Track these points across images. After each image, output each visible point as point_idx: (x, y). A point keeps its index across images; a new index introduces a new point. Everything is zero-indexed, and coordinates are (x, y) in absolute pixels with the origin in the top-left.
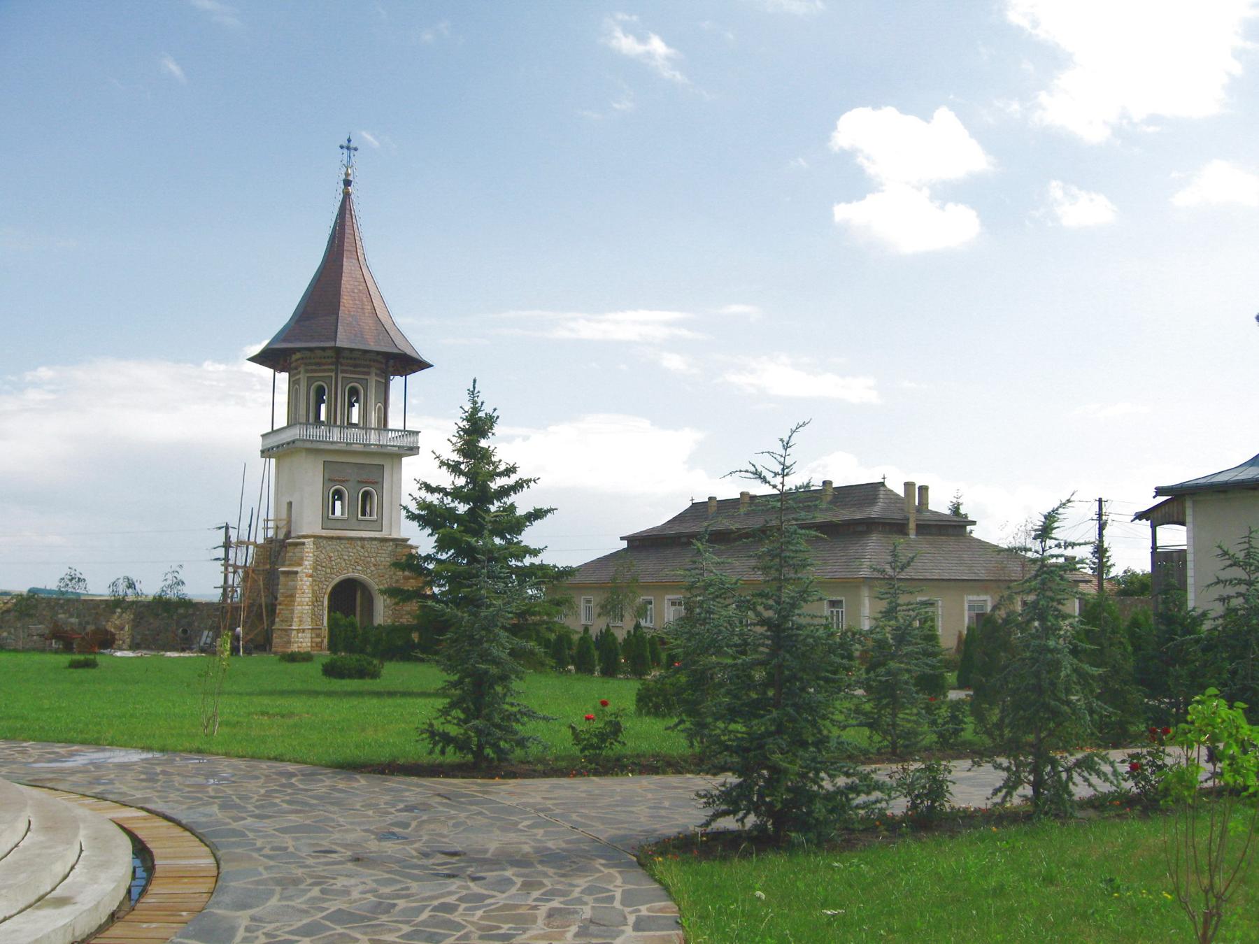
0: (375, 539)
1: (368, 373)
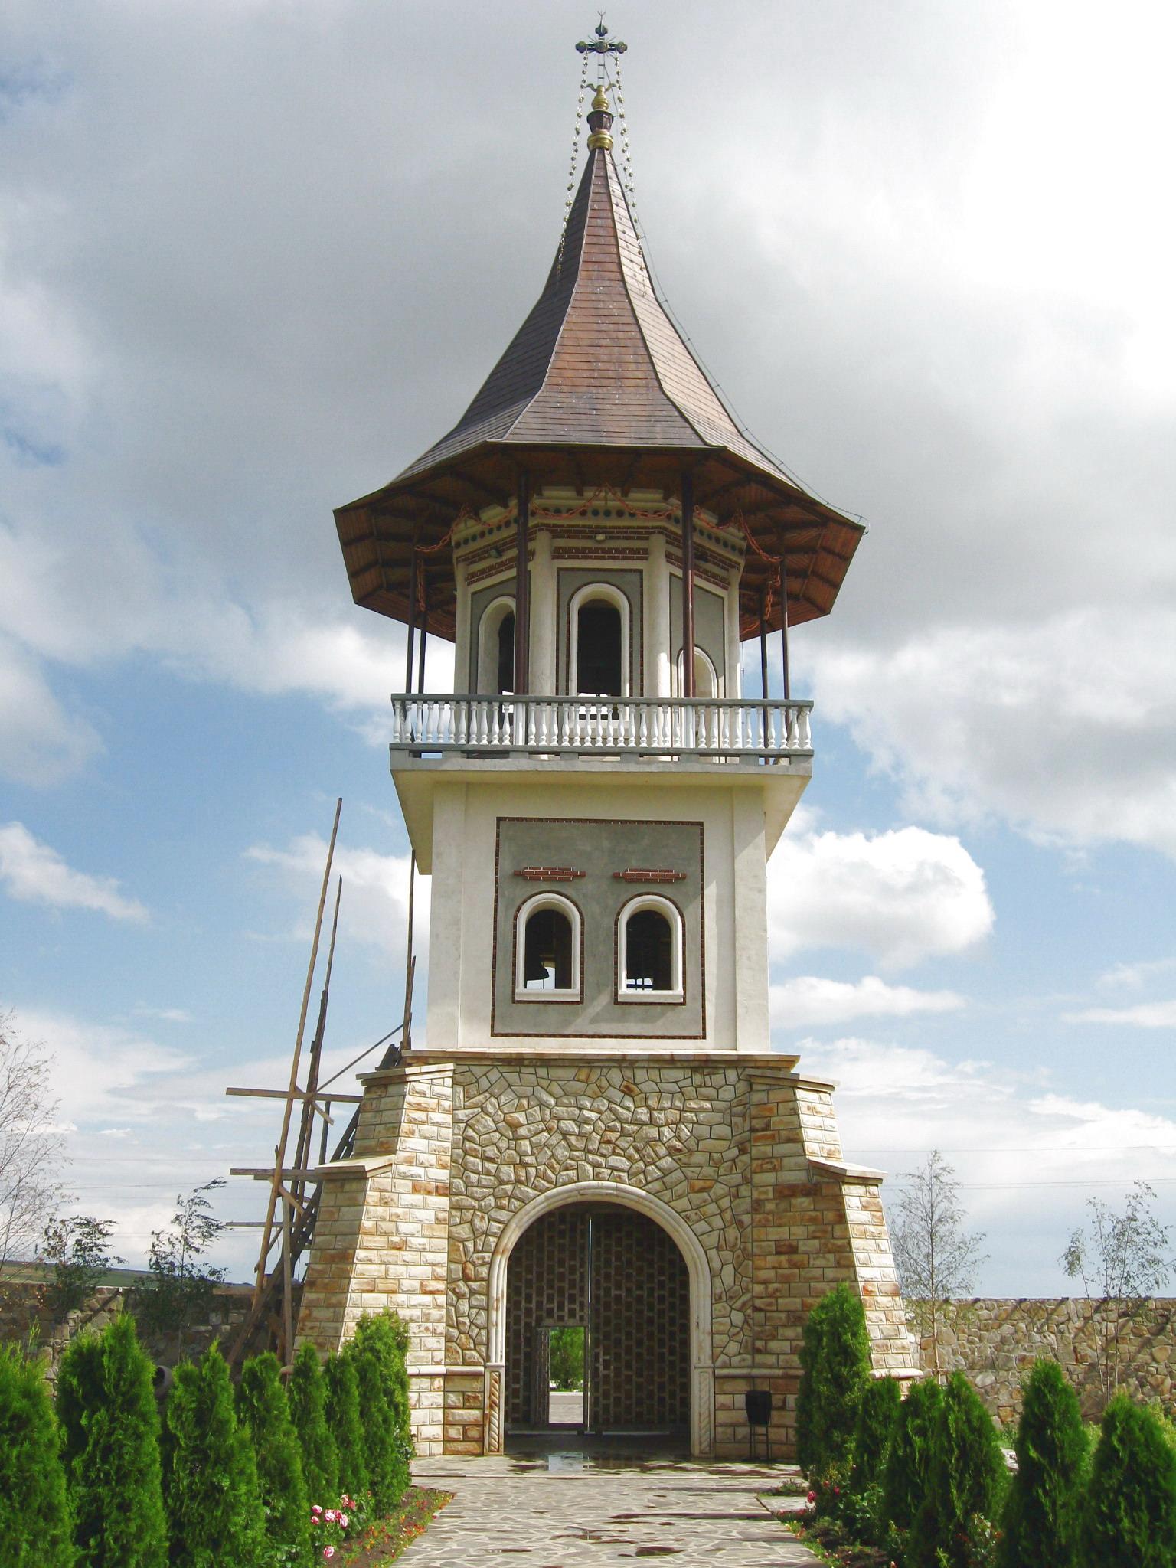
0: (672, 1061)
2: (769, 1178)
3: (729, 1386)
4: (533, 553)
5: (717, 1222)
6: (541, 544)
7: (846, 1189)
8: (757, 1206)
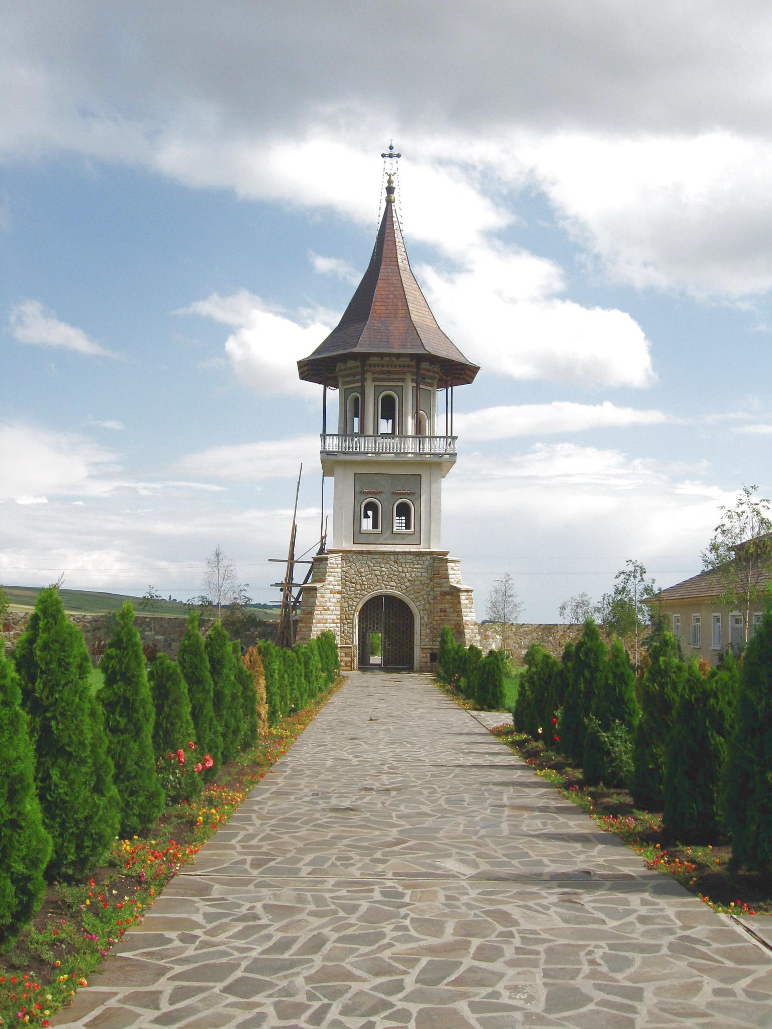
0: (410, 553)
1: (403, 380)
2: (439, 589)
3: (425, 651)
4: (366, 379)
5: (423, 602)
6: (369, 376)
7: (461, 594)
8: (435, 598)
